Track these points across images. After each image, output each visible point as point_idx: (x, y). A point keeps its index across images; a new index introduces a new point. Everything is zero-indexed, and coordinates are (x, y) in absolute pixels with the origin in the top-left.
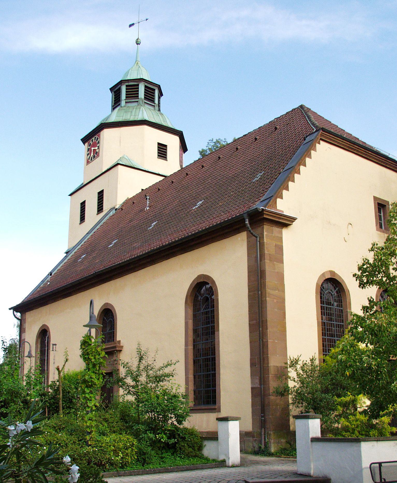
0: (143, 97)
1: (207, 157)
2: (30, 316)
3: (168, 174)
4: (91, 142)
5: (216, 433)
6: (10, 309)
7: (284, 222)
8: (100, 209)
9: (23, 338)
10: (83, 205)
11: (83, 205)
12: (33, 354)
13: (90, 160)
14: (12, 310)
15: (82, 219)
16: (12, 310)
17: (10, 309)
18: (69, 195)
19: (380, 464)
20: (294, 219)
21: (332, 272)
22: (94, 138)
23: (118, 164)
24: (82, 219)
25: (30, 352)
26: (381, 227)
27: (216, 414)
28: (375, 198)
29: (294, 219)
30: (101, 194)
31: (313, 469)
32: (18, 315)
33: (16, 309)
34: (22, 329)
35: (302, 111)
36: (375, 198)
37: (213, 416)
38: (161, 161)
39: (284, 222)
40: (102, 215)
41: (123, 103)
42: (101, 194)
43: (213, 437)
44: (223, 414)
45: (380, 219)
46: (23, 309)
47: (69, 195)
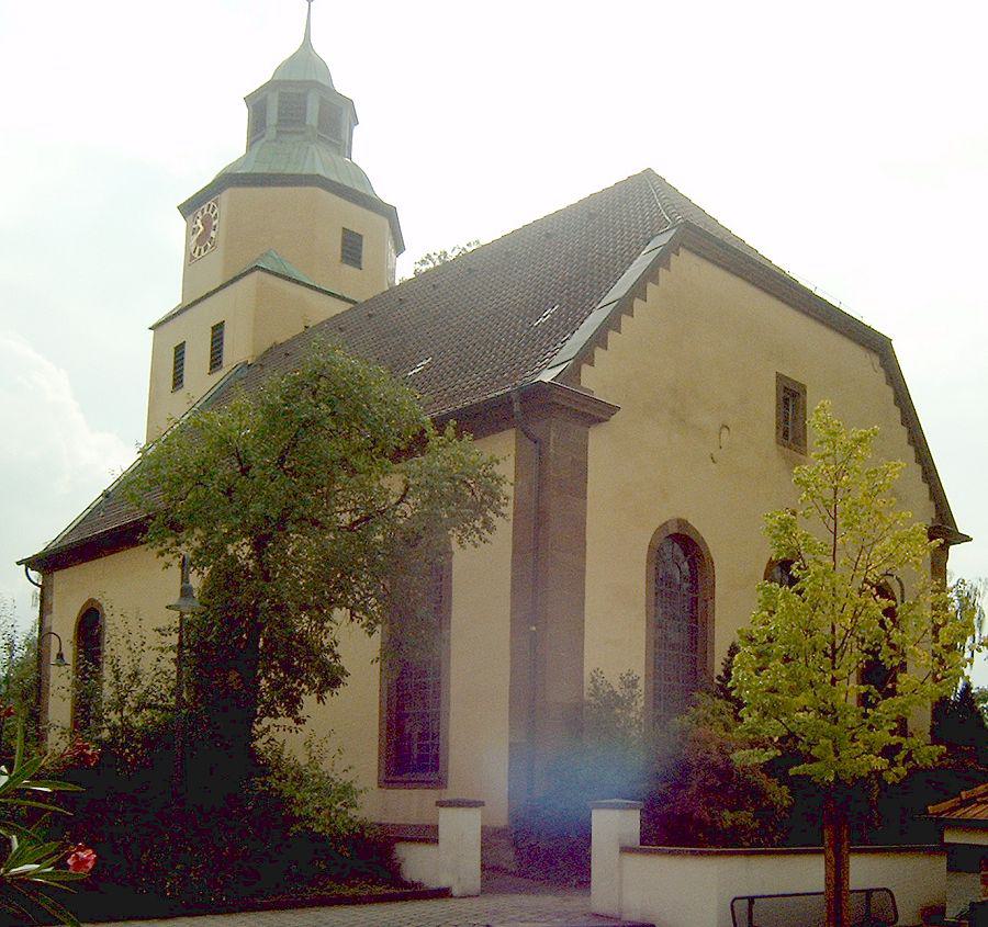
0: (315, 123)
1: (860, 561)
2: (58, 576)
3: (361, 299)
4: (199, 214)
5: (436, 828)
6: (19, 563)
7: (596, 413)
8: (216, 362)
9: (47, 625)
10: (180, 351)
11: (180, 351)
12: (69, 656)
13: (196, 255)
14: (23, 566)
15: (178, 381)
16: (23, 566)
17: (19, 563)
18: (182, 345)
19: (751, 900)
20: (613, 409)
21: (682, 523)
22: (206, 206)
23: (252, 270)
24: (178, 381)
25: (60, 656)
26: (786, 435)
27: (437, 792)
28: (779, 377)
29: (613, 409)
30: (218, 331)
31: (635, 903)
32: (34, 574)
33: (31, 563)
34: (45, 609)
35: (649, 172)
36: (779, 377)
37: (432, 795)
38: (349, 269)
39: (596, 413)
40: (219, 375)
41: (271, 133)
42: (218, 331)
43: (427, 835)
44: (450, 794)
45: (786, 421)
46: (49, 563)
47: (182, 345)
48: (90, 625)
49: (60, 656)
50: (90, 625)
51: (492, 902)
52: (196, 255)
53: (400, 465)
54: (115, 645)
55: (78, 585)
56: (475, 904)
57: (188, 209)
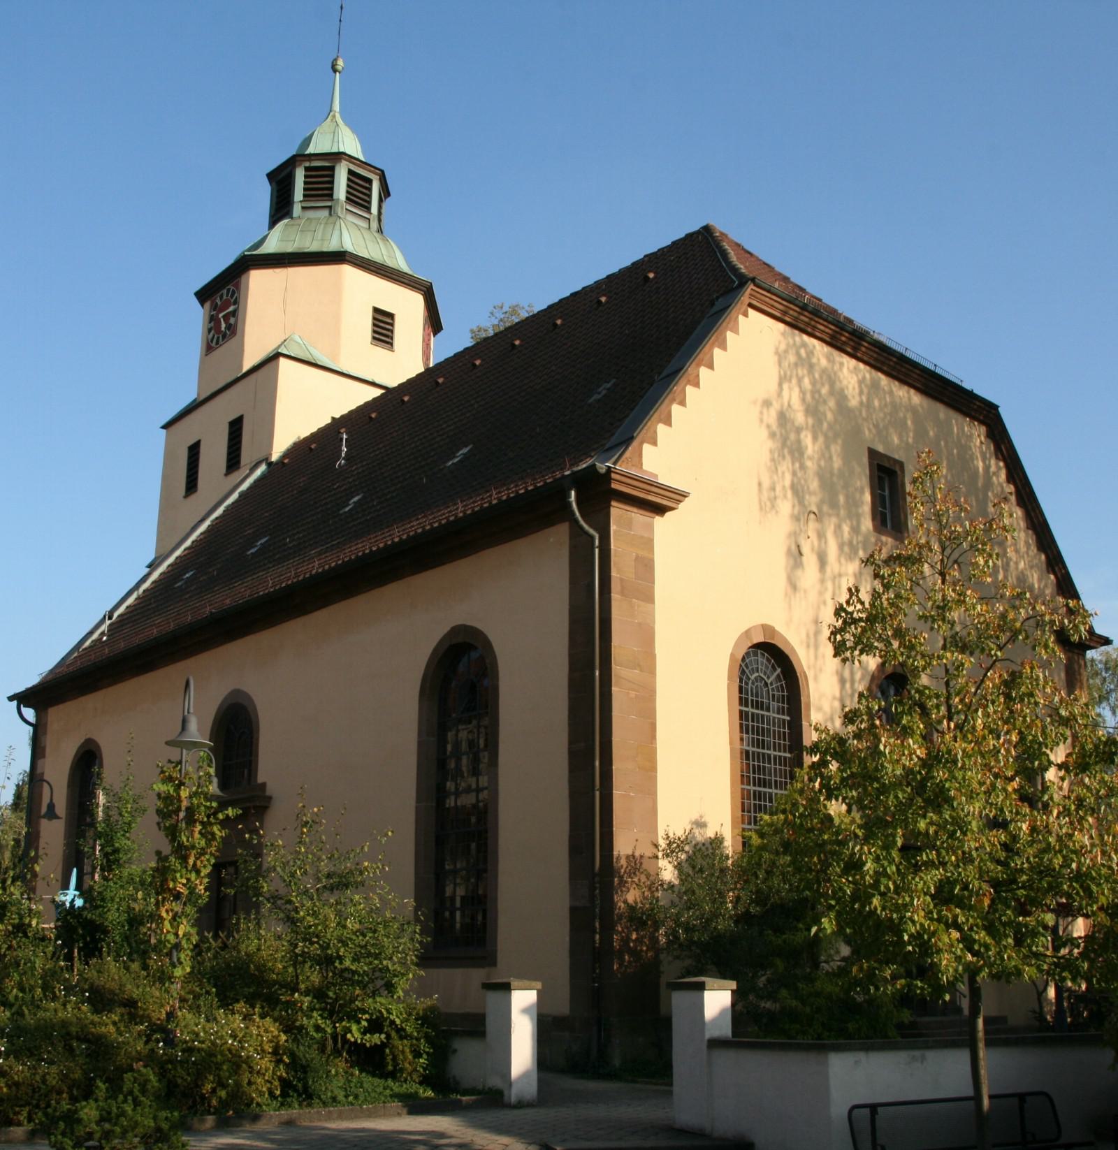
2: (54, 713)
8: (233, 462)
9: (39, 771)
10: (194, 451)
11: (194, 451)
12: (61, 809)
14: (15, 702)
15: (192, 485)
16: (15, 702)
19: (873, 1108)
21: (767, 629)
22: (225, 291)
24: (192, 485)
29: (684, 495)
31: (724, 1117)
32: (29, 713)
33: (23, 699)
37: (477, 975)
38: (380, 352)
46: (40, 698)
48: (87, 761)
49: (51, 806)
50: (87, 761)
51: (207, 610)
52: (213, 344)
53: (831, 664)
54: (111, 769)
55: (77, 721)
56: (530, 1113)
57: (203, 295)
